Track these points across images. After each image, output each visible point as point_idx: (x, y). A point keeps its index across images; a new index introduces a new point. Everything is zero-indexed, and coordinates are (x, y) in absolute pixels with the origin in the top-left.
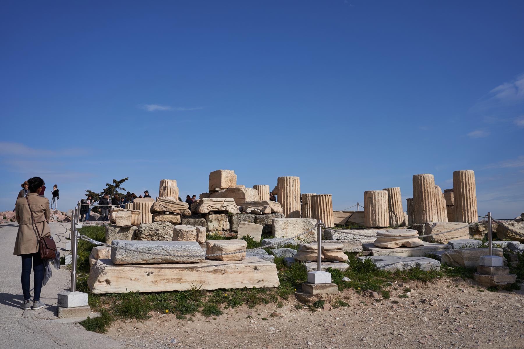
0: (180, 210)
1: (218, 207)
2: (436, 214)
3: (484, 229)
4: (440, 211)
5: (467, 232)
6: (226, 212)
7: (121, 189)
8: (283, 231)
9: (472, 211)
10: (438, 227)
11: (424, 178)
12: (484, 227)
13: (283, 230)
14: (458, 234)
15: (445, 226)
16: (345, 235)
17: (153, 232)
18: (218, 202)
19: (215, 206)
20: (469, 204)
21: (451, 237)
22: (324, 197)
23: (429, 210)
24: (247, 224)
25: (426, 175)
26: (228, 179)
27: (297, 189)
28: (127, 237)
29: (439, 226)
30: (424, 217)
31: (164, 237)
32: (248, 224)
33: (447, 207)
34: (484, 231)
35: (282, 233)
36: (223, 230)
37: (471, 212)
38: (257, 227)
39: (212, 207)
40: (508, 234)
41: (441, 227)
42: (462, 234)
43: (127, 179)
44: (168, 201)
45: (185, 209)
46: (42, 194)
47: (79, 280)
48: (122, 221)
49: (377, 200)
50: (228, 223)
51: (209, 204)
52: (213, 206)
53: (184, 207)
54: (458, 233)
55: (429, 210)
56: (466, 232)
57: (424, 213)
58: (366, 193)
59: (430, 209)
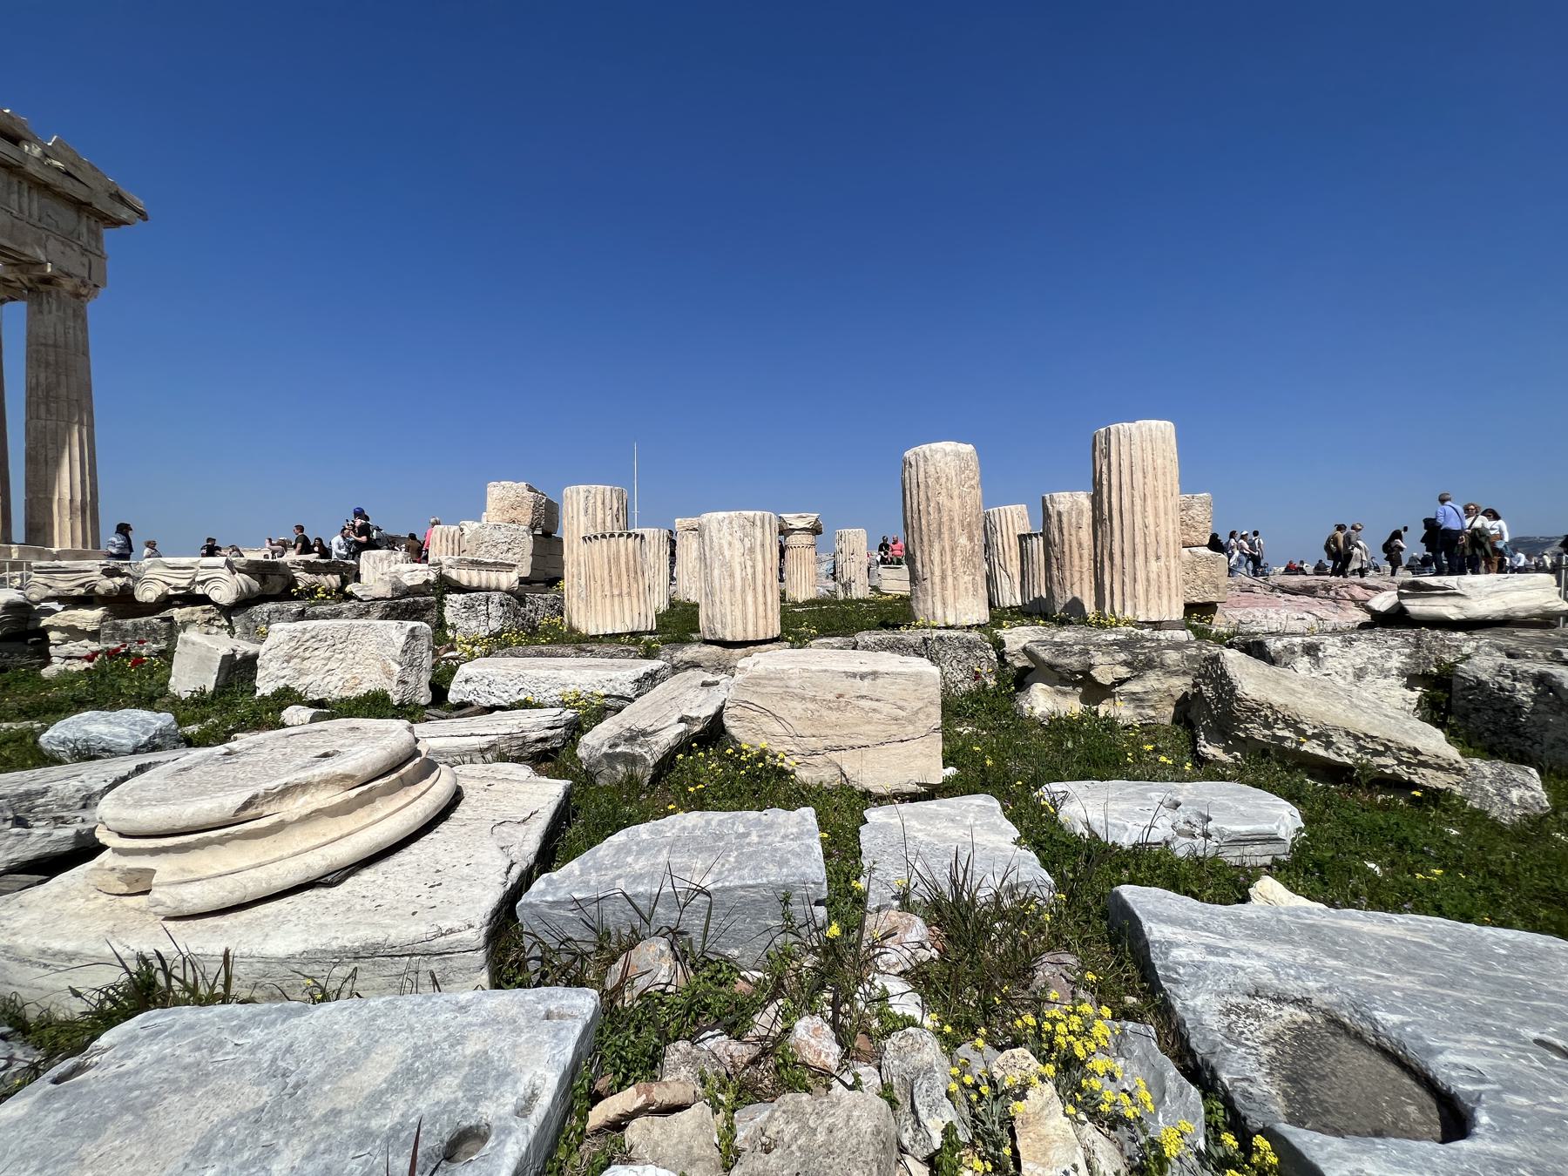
0: (82, 585)
1: (184, 583)
2: (976, 590)
3: (1123, 672)
4: (1082, 579)
5: (928, 716)
8: (285, 665)
9: (1153, 576)
10: (758, 689)
11: (926, 459)
12: (1125, 663)
13: (288, 662)
14: (867, 728)
15: (793, 683)
16: (487, 689)
19: (174, 582)
20: (1140, 548)
21: (828, 743)
23: (943, 578)
25: (934, 446)
27: (599, 520)
29: (758, 685)
30: (925, 602)
33: (554, 573)
34: (1121, 682)
35: (282, 674)
37: (1148, 580)
40: (1240, 729)
41: (769, 689)
42: (894, 729)
49: (716, 544)
54: (869, 723)
55: (943, 578)
56: (921, 716)
57: (926, 589)
59: (949, 572)
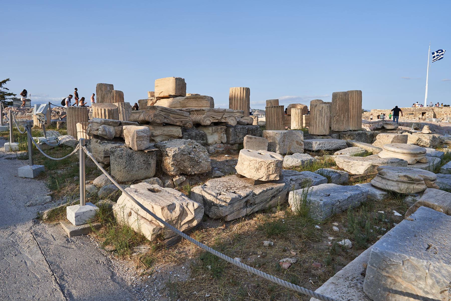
0: (182, 121)
1: (220, 118)
6: (226, 124)
7: (4, 88)
17: (186, 157)
18: (220, 112)
22: (298, 110)
24: (254, 138)
26: (180, 86)
28: (150, 164)
31: (198, 161)
32: (255, 138)
36: (222, 143)
38: (264, 141)
39: (213, 117)
43: (8, 80)
44: (169, 110)
45: (187, 120)
46: (108, 110)
47: (118, 257)
48: (143, 142)
50: (225, 136)
51: (211, 115)
52: (215, 117)
53: (186, 118)
58: (25, 90)
